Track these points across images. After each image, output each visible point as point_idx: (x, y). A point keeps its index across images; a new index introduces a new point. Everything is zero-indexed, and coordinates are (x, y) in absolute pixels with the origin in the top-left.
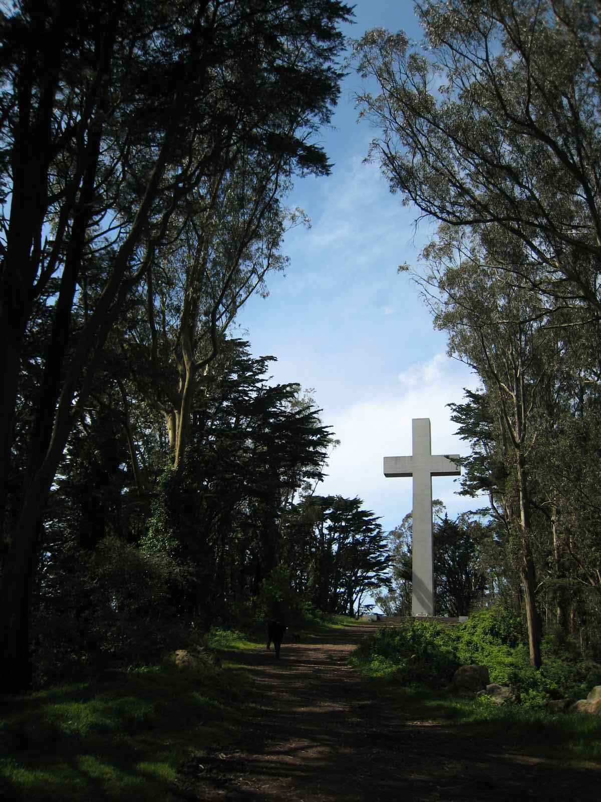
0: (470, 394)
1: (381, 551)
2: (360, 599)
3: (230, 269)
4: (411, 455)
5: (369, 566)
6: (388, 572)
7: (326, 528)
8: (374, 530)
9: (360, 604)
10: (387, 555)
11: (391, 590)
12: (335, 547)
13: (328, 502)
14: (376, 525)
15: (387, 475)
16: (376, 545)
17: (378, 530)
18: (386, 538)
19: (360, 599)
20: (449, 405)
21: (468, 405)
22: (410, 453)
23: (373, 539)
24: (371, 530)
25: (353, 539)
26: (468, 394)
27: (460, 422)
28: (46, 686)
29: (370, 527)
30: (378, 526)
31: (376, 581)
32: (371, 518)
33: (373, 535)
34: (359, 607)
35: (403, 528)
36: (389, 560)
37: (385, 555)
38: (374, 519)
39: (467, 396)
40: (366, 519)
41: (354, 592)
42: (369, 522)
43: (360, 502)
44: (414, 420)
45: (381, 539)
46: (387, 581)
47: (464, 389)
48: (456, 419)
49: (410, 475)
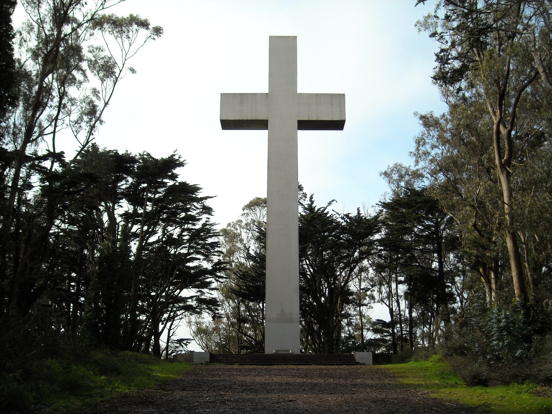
2: (170, 330)
7: (121, 216)
9: (169, 337)
11: (216, 317)
12: (134, 246)
15: (227, 124)
18: (216, 235)
22: (265, 89)
23: (196, 235)
25: (164, 234)
30: (208, 210)
31: (194, 303)
33: (197, 227)
34: (168, 342)
36: (220, 270)
44: (272, 38)
46: (212, 303)
49: (261, 124)
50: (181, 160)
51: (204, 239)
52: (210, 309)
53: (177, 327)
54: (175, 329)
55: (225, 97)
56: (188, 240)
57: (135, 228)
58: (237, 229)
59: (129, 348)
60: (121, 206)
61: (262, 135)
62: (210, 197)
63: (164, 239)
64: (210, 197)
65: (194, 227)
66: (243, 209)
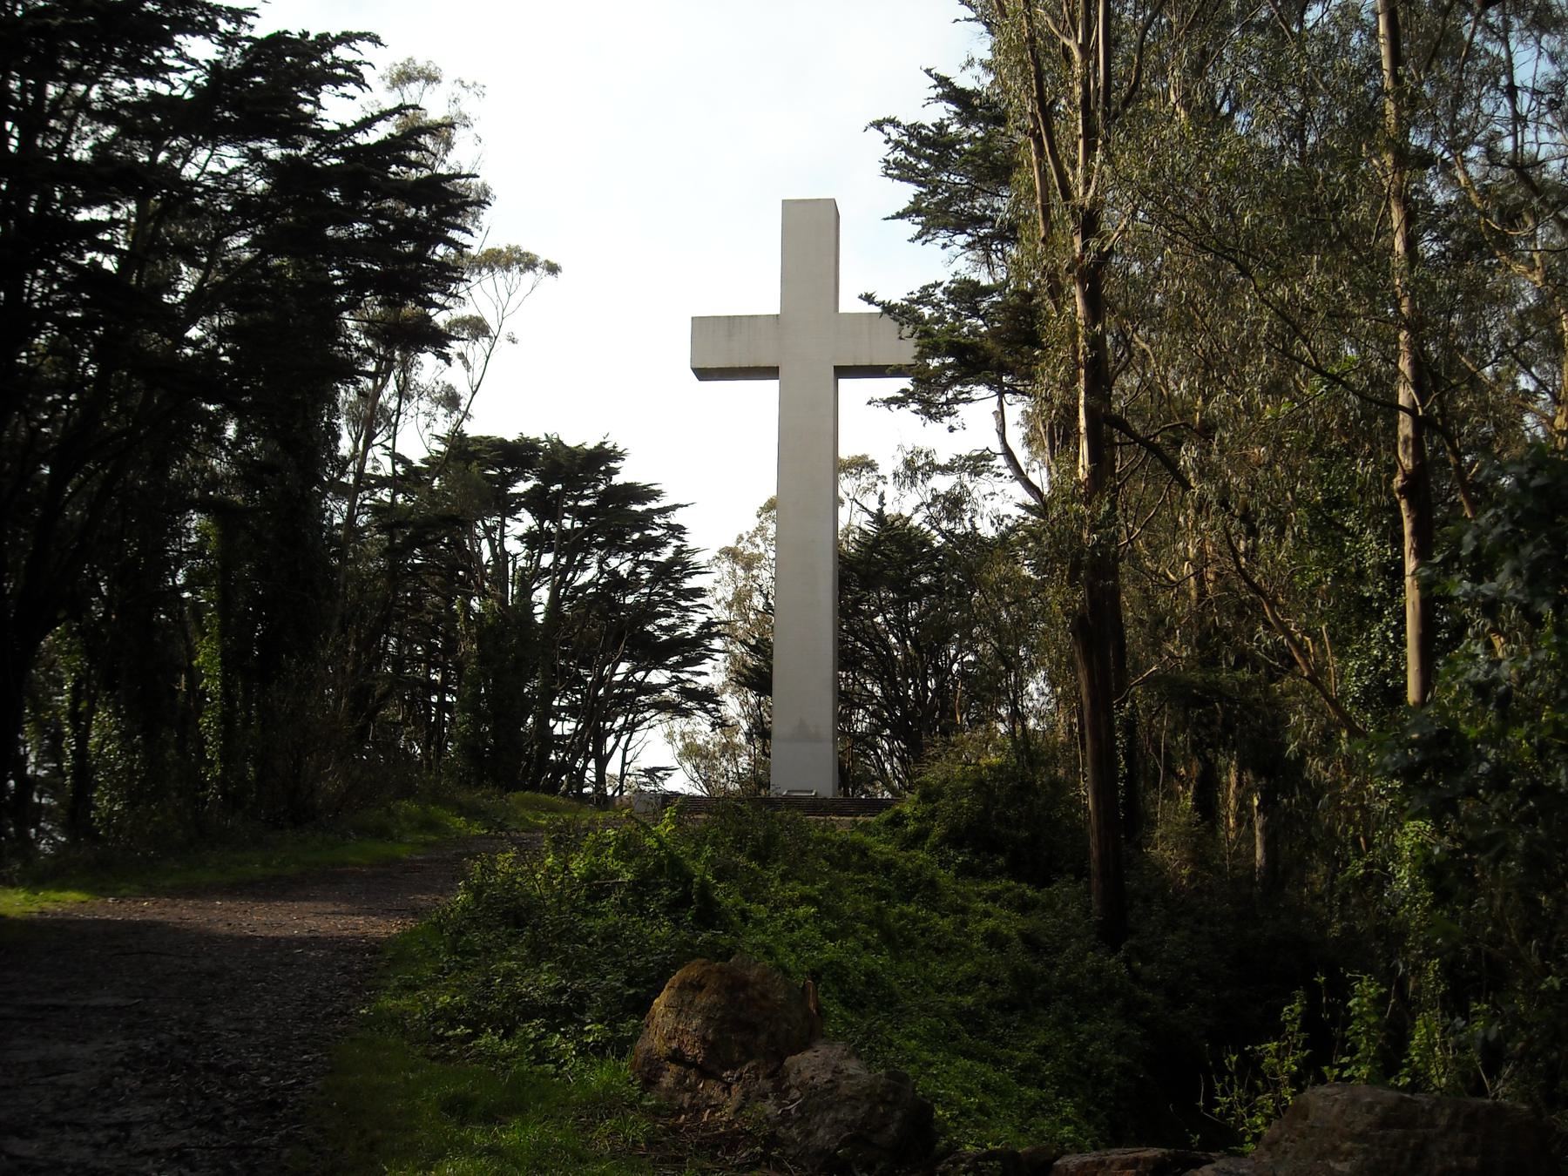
0: (950, 92)
1: (686, 609)
2: (625, 750)
3: (1151, 711)
4: (777, 311)
5: (653, 654)
6: (712, 673)
7: (520, 538)
8: (665, 544)
10: (703, 619)
11: (720, 724)
13: (518, 455)
14: (670, 527)
15: (703, 374)
16: (670, 589)
17: (675, 542)
19: (625, 750)
20: (879, 125)
21: (941, 127)
22: (774, 308)
23: (664, 573)
24: (656, 544)
25: (602, 571)
26: (940, 90)
27: (909, 180)
28: (1239, 779)
29: (654, 533)
30: (677, 530)
32: (653, 505)
33: (662, 559)
35: (758, 540)
37: (700, 619)
38: (663, 511)
39: (939, 98)
40: (638, 508)
41: (611, 731)
42: (645, 520)
43: (619, 456)
44: (787, 204)
45: (690, 570)
46: (706, 698)
47: (928, 71)
48: (902, 172)
49: (770, 372)
50: (619, 450)
51: (677, 581)
52: (707, 711)
53: (642, 744)
54: (638, 749)
55: (702, 326)
56: (649, 580)
57: (547, 560)
58: (758, 546)
59: (534, 786)
60: (520, 520)
61: (770, 388)
62: (682, 506)
63: (601, 581)
64: (682, 506)
65: (656, 559)
66: (759, 516)
